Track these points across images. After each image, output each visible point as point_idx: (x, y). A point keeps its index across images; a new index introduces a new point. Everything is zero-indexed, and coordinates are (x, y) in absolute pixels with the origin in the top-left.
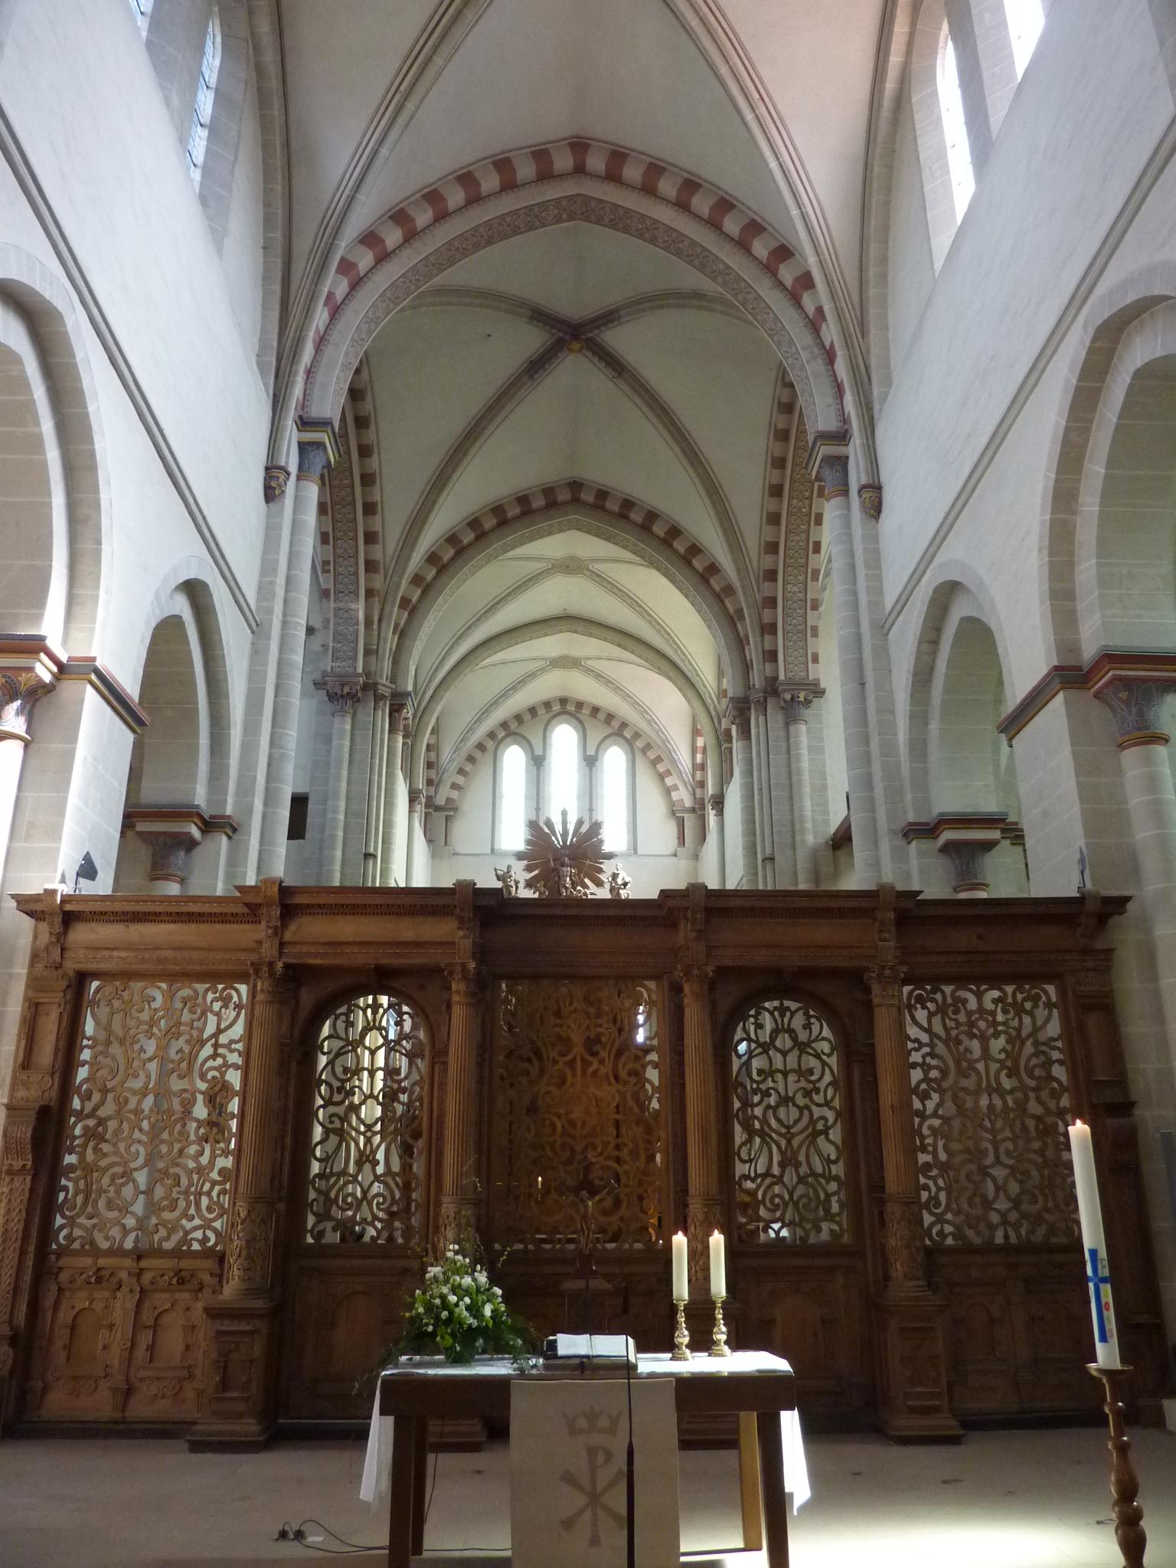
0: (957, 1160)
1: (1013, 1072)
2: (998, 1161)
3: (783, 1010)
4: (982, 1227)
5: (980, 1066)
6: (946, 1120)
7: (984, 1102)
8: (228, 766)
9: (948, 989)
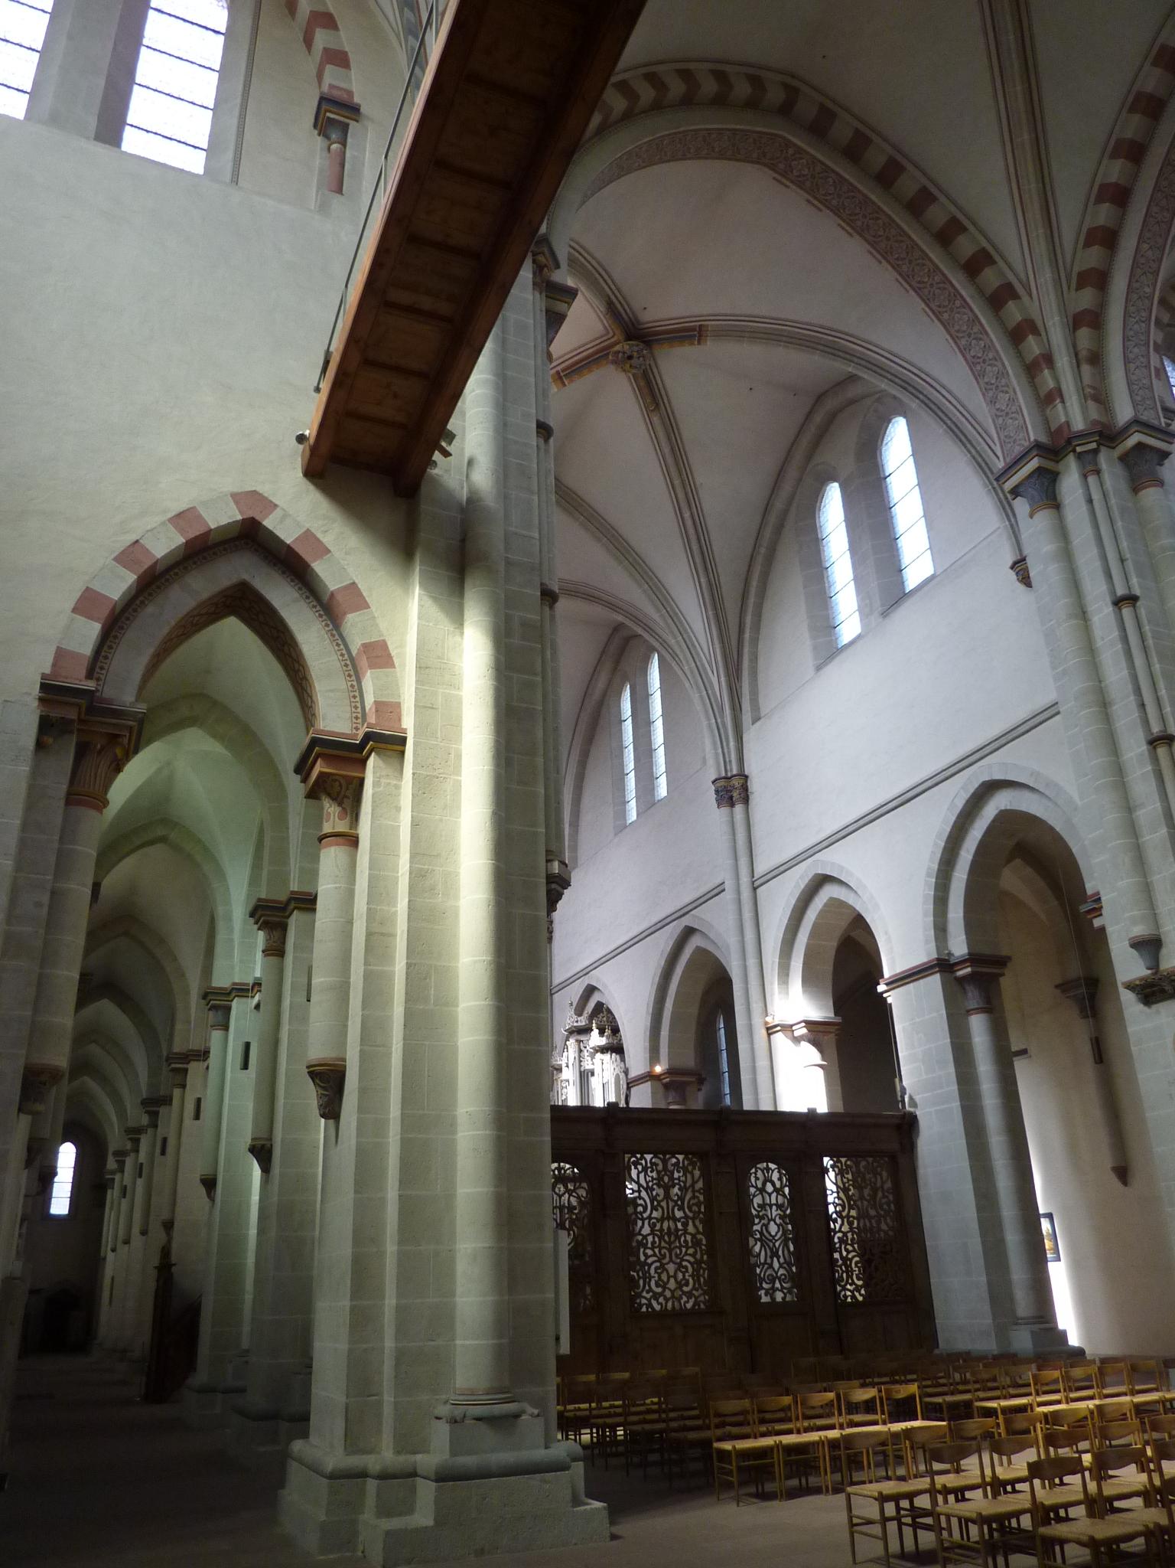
0: (650, 1261)
1: (874, 1207)
2: (671, 1260)
3: (768, 1169)
4: (661, 1300)
5: (664, 1204)
6: (845, 1234)
7: (665, 1225)
8: (390, 1018)
9: (648, 1157)
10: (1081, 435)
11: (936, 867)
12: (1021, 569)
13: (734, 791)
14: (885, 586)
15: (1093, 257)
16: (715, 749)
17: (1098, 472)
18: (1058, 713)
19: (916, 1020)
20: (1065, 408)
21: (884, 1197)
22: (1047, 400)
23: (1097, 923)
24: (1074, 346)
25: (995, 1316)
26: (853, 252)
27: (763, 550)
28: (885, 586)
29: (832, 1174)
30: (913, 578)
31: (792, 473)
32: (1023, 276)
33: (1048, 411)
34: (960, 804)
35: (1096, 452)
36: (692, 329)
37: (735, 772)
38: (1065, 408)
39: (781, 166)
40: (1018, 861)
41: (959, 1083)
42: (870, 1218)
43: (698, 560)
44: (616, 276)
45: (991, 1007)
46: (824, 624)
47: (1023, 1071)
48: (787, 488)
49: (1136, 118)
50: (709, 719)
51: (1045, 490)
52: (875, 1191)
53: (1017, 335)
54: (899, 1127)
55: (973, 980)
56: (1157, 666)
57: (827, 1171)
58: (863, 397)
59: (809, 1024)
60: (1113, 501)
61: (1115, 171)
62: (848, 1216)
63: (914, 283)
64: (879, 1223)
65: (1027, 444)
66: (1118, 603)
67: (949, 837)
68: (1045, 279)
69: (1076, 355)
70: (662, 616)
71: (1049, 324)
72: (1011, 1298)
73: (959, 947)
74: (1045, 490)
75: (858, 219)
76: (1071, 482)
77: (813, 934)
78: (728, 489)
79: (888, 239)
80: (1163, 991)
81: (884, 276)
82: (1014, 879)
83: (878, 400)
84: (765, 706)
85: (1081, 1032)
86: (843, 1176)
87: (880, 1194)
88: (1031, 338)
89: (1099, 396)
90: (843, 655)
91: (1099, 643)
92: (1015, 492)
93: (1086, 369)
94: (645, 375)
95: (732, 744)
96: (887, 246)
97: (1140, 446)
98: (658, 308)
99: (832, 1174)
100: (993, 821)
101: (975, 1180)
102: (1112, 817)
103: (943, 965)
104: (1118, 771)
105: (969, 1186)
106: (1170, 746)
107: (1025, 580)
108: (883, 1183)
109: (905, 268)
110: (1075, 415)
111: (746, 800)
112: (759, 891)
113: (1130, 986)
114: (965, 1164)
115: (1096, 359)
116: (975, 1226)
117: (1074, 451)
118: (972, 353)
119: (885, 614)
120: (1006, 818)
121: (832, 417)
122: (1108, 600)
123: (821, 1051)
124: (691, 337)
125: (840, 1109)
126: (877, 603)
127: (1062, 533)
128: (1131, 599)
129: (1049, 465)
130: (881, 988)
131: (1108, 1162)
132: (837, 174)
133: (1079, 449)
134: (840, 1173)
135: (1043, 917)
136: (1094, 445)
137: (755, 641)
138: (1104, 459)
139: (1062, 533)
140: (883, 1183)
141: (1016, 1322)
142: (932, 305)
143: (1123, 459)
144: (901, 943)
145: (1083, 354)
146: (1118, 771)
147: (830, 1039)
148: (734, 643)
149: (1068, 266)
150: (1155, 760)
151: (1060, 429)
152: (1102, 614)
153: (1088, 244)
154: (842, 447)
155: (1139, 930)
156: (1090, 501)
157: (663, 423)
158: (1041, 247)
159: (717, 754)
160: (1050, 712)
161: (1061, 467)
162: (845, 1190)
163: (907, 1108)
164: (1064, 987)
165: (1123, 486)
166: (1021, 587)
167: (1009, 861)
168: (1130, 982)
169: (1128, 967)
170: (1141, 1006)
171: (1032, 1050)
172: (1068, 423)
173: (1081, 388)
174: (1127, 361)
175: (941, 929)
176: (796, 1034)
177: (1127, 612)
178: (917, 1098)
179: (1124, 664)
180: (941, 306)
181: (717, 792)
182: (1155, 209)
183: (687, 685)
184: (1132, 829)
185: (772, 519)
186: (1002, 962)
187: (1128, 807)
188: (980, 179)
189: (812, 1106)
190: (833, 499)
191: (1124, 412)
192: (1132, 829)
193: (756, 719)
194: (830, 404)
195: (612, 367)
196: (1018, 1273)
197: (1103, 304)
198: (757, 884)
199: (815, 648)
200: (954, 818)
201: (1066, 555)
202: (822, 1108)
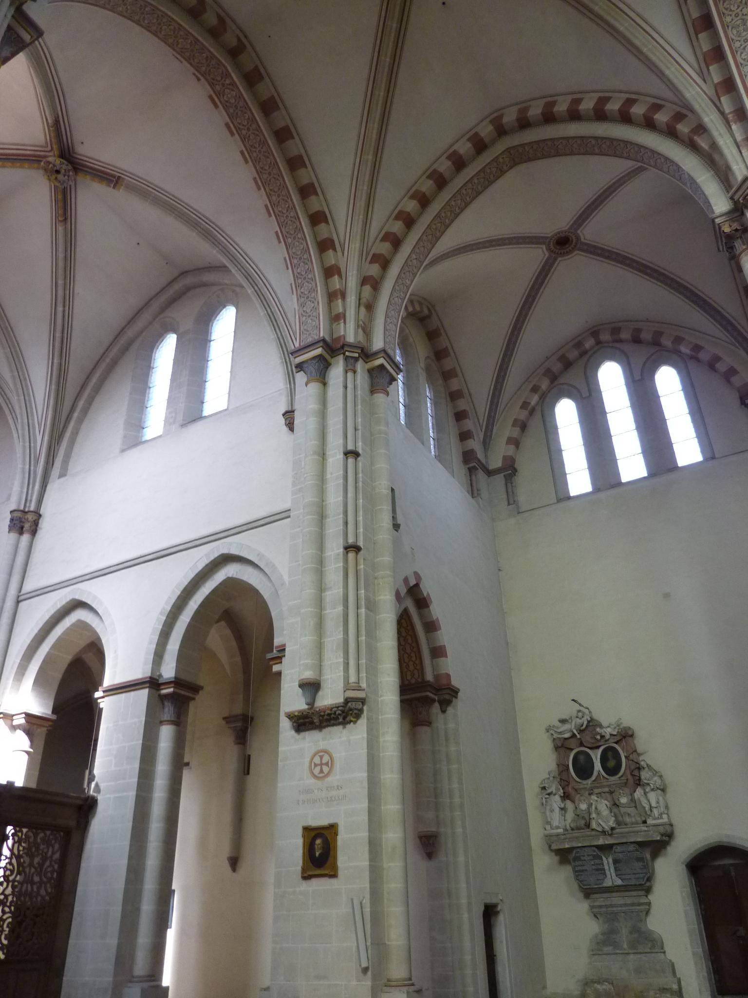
1: (39, 874)
10: (350, 345)
11: (169, 608)
12: (289, 417)
13: (26, 523)
14: (189, 408)
15: (384, 248)
16: (22, 487)
17: (355, 372)
18: (289, 517)
19: (119, 722)
20: (345, 327)
21: (51, 865)
22: (337, 318)
23: (276, 668)
24: (360, 294)
25: (116, 974)
26: (241, 176)
27: (108, 360)
28: (189, 408)
29: (10, 842)
30: (208, 409)
31: (146, 316)
32: (342, 241)
33: (334, 325)
34: (200, 566)
35: (356, 359)
36: (114, 176)
37: (32, 509)
38: (345, 327)
39: (218, 88)
40: (223, 623)
41: (139, 778)
42: (32, 883)
43: (57, 344)
44: (69, 102)
45: (179, 722)
46: (136, 423)
47: (188, 778)
48: (140, 324)
49: (430, 183)
50: (24, 464)
51: (320, 370)
52: (44, 859)
53: (330, 272)
54: (80, 808)
55: (170, 699)
56: (361, 501)
57: (8, 838)
58: (213, 284)
59: (29, 716)
60: (359, 392)
61: (411, 206)
62: (14, 881)
63: (276, 211)
64: (39, 889)
65: (316, 338)
66: (347, 453)
67: (185, 589)
68: (355, 246)
69: (360, 299)
70: (13, 377)
71: (349, 274)
72: (132, 957)
73: (168, 671)
74: (320, 370)
75: (254, 153)
76: (337, 372)
77: (54, 647)
78: (96, 307)
79: (270, 174)
80: (312, 723)
81: (258, 200)
82: (218, 639)
83: (222, 290)
84: (73, 467)
85: (232, 752)
86: (20, 844)
87: (48, 863)
88: (336, 277)
89: (366, 329)
90: (145, 445)
91: (329, 476)
92: (300, 367)
93: (363, 310)
94: (64, 192)
95: (37, 487)
96: (266, 179)
97: (382, 366)
98: (92, 148)
99: (10, 842)
100: (220, 584)
101: (130, 858)
102: (309, 591)
103: (153, 683)
104: (320, 562)
105: (125, 862)
106: (357, 553)
107: (290, 426)
108: (53, 853)
109: (274, 198)
110: (350, 332)
111: (34, 532)
112: (21, 604)
113: (290, 716)
114: (127, 843)
115: (370, 307)
116: (120, 896)
117: (344, 354)
118: (299, 271)
119: (183, 426)
120: (231, 584)
121: (187, 290)
122: (342, 450)
123: (31, 741)
124: (111, 181)
125: (33, 785)
126: (180, 418)
127: (323, 401)
128: (356, 454)
129: (327, 356)
130: (97, 694)
131: (226, 850)
132: (252, 114)
133: (347, 353)
134: (18, 842)
135: (227, 667)
136: (356, 355)
137: (80, 421)
138: (360, 366)
139: (323, 401)
140: (53, 853)
141: (132, 979)
142: (283, 230)
143: (370, 371)
144: (126, 656)
145: (364, 300)
146: (320, 562)
147: (42, 732)
148: (63, 420)
149: (370, 244)
150: (346, 561)
151: (339, 338)
152: (335, 457)
153: (383, 240)
154: (185, 313)
155: (308, 675)
156: (346, 387)
157: (66, 236)
158: (358, 227)
159: (22, 492)
160: (284, 515)
161: (332, 361)
162: (18, 857)
163: (91, 793)
164: (227, 719)
165: (367, 387)
166: (285, 429)
167: (218, 621)
168: (293, 713)
169: (292, 700)
170: (293, 732)
171: (192, 764)
172: (344, 336)
173: (357, 320)
174: (387, 316)
175: (159, 656)
176: (15, 723)
177: (351, 461)
178: (102, 786)
179: (341, 493)
180: (287, 234)
181: (12, 520)
182: (425, 237)
183: (15, 435)
184: (320, 603)
185: (123, 341)
186: (196, 689)
187: (321, 588)
188: (336, 168)
189: (11, 779)
190: (169, 345)
191: (378, 343)
192: (320, 603)
193: (62, 475)
194: (188, 281)
195: (41, 172)
196: (144, 938)
197: (382, 277)
198: (21, 598)
199: (125, 437)
200: (186, 583)
201: (323, 414)
202: (19, 783)
